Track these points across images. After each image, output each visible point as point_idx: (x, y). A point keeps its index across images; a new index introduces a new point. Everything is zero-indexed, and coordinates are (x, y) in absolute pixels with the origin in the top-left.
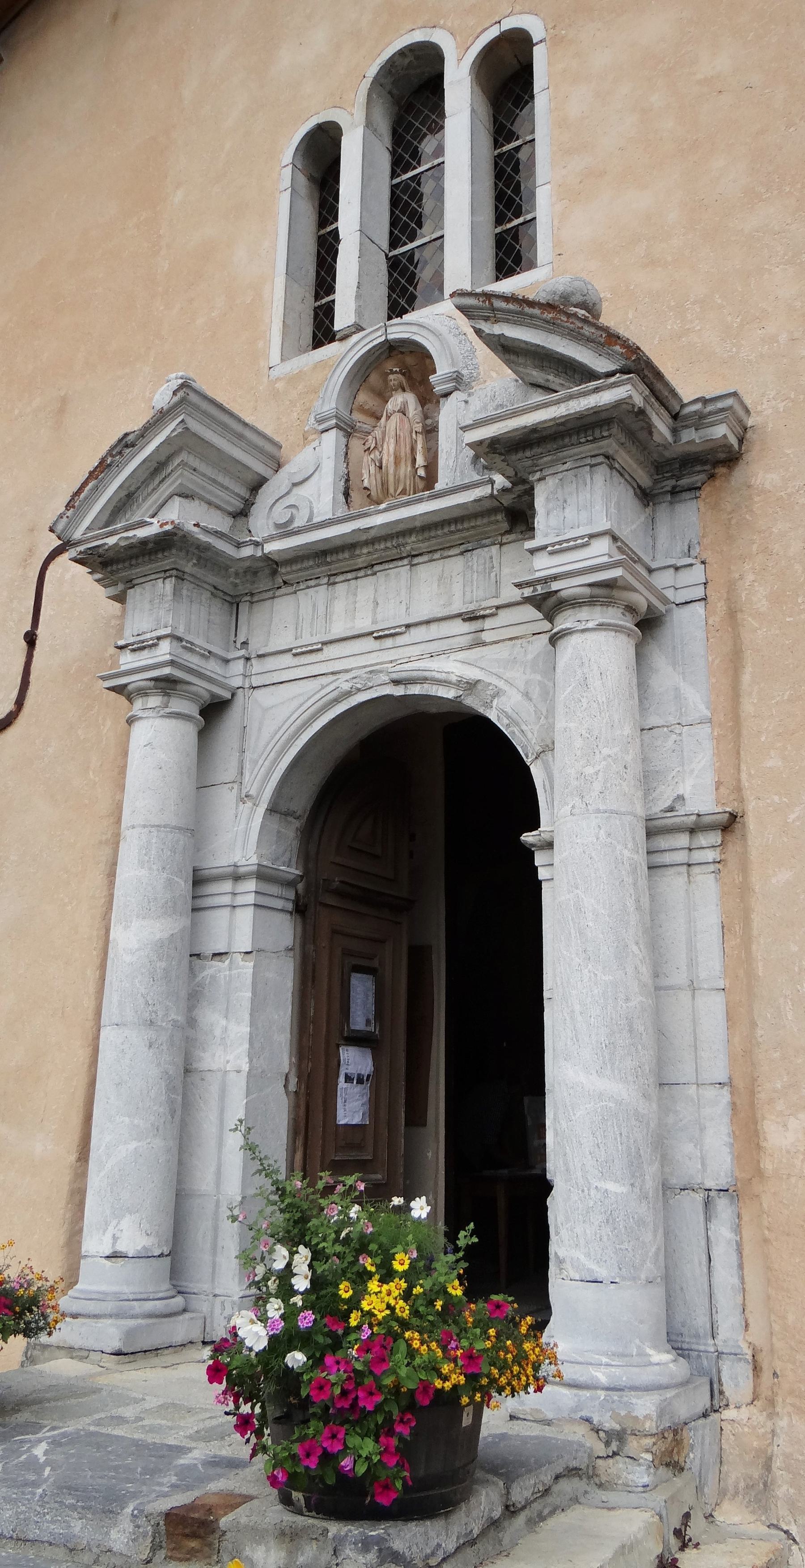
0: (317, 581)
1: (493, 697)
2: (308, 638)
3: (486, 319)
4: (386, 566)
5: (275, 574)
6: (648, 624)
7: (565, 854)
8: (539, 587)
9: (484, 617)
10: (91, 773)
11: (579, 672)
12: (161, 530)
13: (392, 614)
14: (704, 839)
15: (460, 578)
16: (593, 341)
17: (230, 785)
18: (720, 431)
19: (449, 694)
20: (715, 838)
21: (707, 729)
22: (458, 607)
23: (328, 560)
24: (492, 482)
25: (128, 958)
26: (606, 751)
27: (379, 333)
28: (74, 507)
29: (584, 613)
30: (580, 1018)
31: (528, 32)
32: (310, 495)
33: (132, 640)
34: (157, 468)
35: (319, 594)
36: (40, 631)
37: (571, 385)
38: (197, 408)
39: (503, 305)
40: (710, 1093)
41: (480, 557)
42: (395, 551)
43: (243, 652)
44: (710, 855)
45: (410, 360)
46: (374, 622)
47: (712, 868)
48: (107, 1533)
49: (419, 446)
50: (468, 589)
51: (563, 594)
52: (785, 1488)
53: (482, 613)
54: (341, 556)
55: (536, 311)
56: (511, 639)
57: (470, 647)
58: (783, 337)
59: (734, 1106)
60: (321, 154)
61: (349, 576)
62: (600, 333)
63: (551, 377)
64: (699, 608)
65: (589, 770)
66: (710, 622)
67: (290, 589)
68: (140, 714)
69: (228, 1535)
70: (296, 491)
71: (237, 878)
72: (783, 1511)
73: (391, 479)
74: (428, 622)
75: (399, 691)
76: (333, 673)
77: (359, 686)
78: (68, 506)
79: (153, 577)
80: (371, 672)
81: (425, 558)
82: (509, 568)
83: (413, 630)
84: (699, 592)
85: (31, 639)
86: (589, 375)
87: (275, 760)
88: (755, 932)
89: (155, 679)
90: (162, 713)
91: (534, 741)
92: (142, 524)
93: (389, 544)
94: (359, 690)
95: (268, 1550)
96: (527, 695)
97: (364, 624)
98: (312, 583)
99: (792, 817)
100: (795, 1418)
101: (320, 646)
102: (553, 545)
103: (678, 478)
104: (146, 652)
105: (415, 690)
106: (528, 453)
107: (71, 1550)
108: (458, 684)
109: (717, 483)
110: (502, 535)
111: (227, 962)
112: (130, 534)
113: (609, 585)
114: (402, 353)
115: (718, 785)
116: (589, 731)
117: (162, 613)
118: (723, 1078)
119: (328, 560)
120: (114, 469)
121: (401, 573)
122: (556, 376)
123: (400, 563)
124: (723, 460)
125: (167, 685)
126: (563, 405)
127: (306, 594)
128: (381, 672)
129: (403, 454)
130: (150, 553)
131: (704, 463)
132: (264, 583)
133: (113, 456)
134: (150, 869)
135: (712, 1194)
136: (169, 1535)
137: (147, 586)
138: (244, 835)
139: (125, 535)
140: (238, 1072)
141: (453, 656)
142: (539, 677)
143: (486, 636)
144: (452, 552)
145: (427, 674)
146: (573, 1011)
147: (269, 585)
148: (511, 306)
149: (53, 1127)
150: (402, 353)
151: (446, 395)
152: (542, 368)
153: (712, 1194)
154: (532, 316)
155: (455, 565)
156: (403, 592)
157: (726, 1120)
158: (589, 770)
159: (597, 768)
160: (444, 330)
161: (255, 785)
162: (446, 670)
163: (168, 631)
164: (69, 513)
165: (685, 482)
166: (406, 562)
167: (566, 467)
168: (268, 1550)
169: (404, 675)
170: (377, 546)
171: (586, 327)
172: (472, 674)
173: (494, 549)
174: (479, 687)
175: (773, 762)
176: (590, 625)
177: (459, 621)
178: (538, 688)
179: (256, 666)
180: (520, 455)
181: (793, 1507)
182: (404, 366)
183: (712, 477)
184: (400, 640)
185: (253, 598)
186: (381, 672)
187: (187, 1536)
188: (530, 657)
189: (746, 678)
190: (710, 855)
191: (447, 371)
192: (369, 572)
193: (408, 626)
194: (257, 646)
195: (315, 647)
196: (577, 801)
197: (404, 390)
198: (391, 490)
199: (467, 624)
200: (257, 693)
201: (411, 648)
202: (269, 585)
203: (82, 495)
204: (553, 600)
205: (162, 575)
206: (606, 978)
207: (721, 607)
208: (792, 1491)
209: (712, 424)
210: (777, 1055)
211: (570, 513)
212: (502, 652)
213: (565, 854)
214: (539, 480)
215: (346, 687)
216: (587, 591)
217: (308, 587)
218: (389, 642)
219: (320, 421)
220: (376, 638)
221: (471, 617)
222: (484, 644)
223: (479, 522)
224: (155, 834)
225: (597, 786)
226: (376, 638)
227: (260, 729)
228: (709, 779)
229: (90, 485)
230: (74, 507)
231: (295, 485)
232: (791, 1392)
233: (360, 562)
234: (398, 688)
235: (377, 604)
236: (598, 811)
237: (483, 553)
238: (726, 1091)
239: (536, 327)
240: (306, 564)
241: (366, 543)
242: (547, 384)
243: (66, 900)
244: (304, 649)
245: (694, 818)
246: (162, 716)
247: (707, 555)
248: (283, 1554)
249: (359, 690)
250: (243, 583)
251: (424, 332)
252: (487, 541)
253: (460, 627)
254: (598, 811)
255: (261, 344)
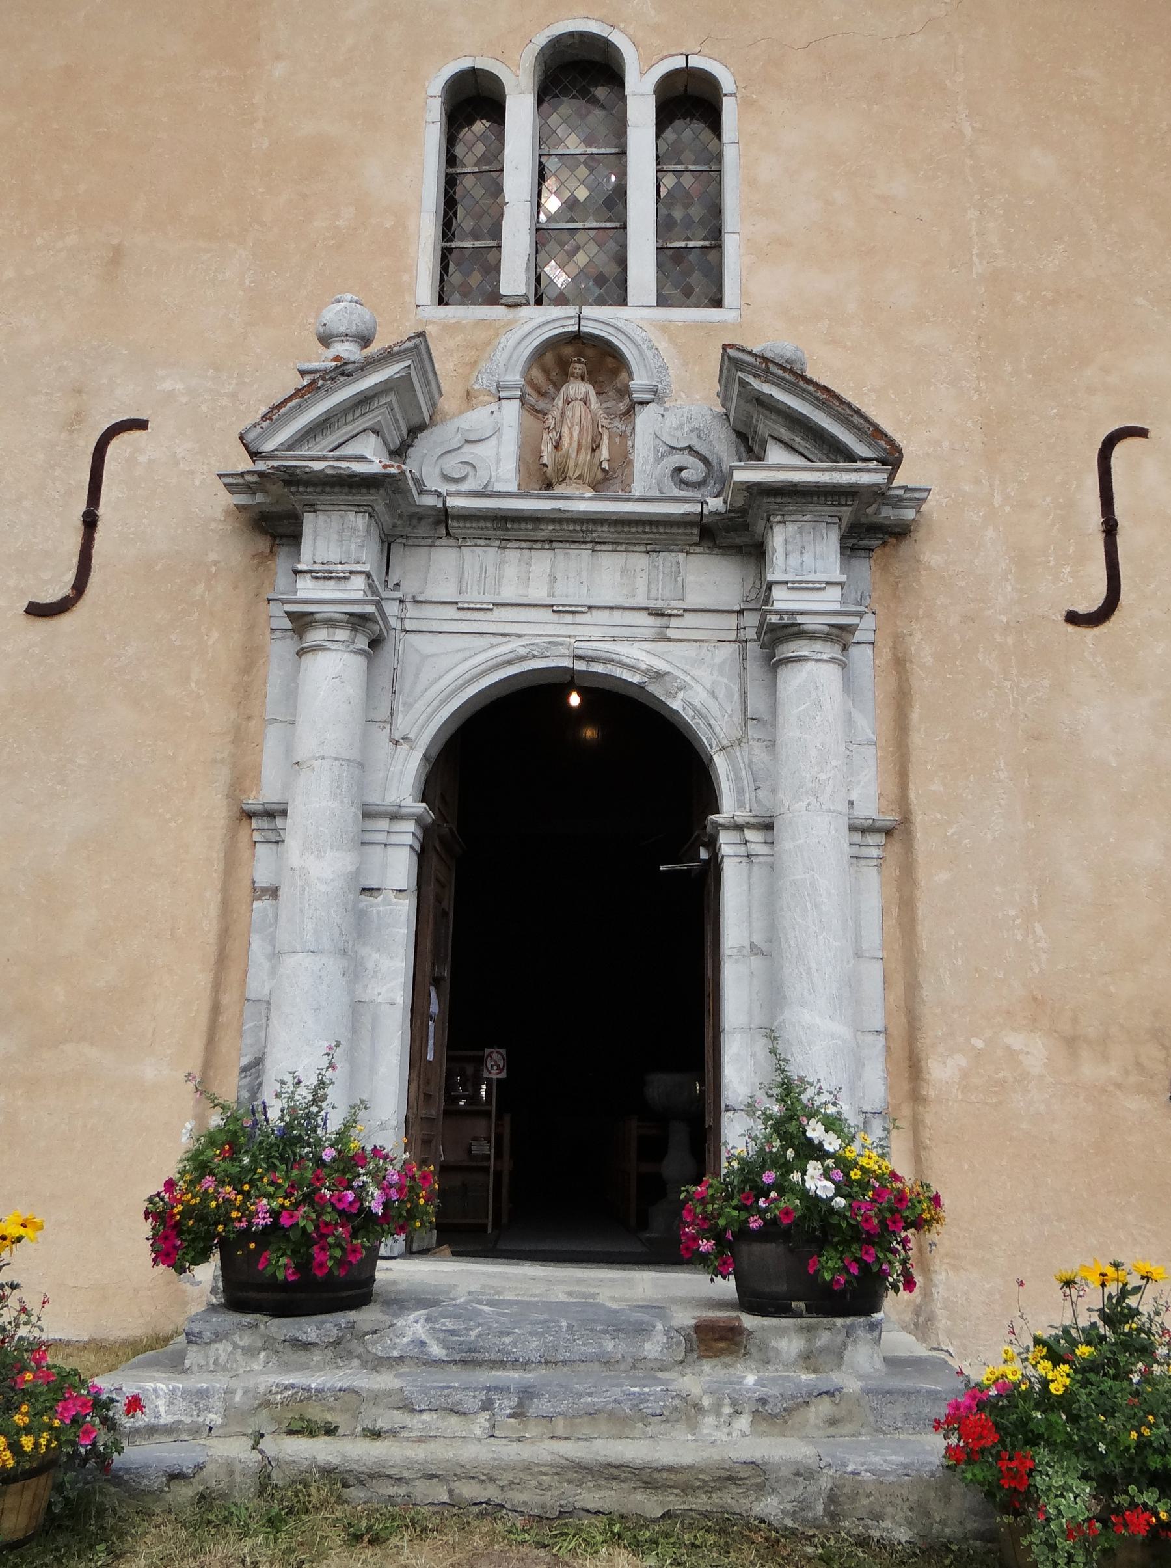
0: (487, 542)
1: (680, 689)
2: (473, 595)
3: (756, 376)
4: (567, 545)
5: (446, 524)
6: (375, 643)
7: (800, 841)
8: (785, 617)
9: (670, 615)
10: (193, 685)
11: (814, 694)
12: (384, 471)
13: (570, 593)
14: (871, 839)
15: (645, 574)
16: (859, 429)
17: (382, 725)
18: (910, 514)
19: (636, 679)
20: (880, 839)
21: (872, 749)
22: (641, 601)
23: (509, 526)
24: (703, 503)
25: (323, 888)
26: (834, 763)
27: (572, 322)
28: (271, 419)
29: (818, 646)
30: (815, 974)
31: (716, 79)
32: (483, 450)
33: (317, 567)
34: (363, 401)
35: (489, 555)
36: (103, 511)
37: (824, 458)
38: (419, 354)
39: (780, 372)
40: (870, 1038)
41: (666, 560)
42: (568, 534)
43: (398, 595)
44: (875, 852)
45: (590, 352)
46: (551, 595)
47: (875, 862)
48: (642, 1346)
49: (605, 440)
50: (653, 586)
51: (806, 627)
52: (943, 1322)
53: (669, 611)
54: (523, 526)
55: (811, 388)
56: (696, 641)
57: (654, 640)
58: (946, 445)
59: (888, 1048)
60: (473, 101)
61: (523, 545)
62: (867, 425)
63: (798, 439)
64: (868, 650)
65: (822, 776)
66: (877, 662)
67: (453, 542)
68: (328, 644)
69: (756, 1334)
70: (468, 448)
71: (395, 817)
72: (942, 1337)
73: (572, 463)
74: (611, 608)
75: (580, 666)
76: (502, 635)
77: (536, 653)
78: (264, 418)
79: (343, 508)
80: (550, 643)
81: (609, 547)
82: (710, 581)
83: (594, 612)
84: (869, 637)
85: (90, 522)
86: (851, 457)
87: (438, 707)
88: (920, 916)
89: (350, 614)
90: (351, 647)
91: (722, 735)
92: (361, 459)
93: (578, 528)
94: (534, 657)
95: (790, 1341)
96: (713, 694)
97: (538, 593)
98: (482, 542)
99: (950, 832)
100: (950, 1273)
101: (491, 606)
102: (793, 582)
103: (861, 539)
104: (332, 582)
105: (599, 668)
106: (779, 500)
107: (605, 1363)
108: (645, 673)
109: (887, 549)
110: (690, 545)
111: (380, 898)
112: (344, 465)
113: (841, 627)
114: (583, 343)
115: (880, 795)
116: (822, 744)
117: (353, 546)
118: (880, 1027)
119: (509, 526)
120: (322, 393)
121: (582, 555)
122: (803, 439)
123: (583, 546)
124: (900, 532)
125: (357, 621)
126: (827, 473)
127: (473, 552)
128: (561, 644)
129: (584, 442)
130: (350, 486)
131: (885, 533)
132: (423, 530)
133: (324, 379)
134: (342, 802)
135: (868, 1115)
136: (700, 1340)
137: (335, 516)
138: (401, 779)
139: (335, 464)
140: (392, 1004)
141: (637, 644)
142: (726, 681)
143: (670, 633)
144: (636, 548)
145: (615, 657)
146: (810, 968)
147: (431, 534)
148: (786, 376)
149: (169, 1052)
150: (583, 343)
151: (643, 403)
152: (791, 429)
153: (868, 1115)
154: (804, 390)
155: (639, 561)
156: (584, 574)
157: (882, 1059)
158: (822, 776)
159: (829, 775)
160: (638, 339)
161: (415, 729)
162: (631, 655)
163: (366, 568)
164: (264, 425)
165: (864, 543)
166: (589, 546)
167: (805, 518)
168: (790, 1341)
169: (590, 653)
170: (564, 526)
171: (855, 417)
172: (662, 666)
173: (681, 556)
174: (667, 678)
175: (936, 787)
176: (825, 657)
177: (645, 613)
178: (724, 690)
179: (411, 611)
180: (772, 499)
181: (950, 1334)
182: (586, 358)
183: (884, 543)
184: (580, 618)
185: (409, 541)
186: (561, 644)
187: (716, 1340)
188: (717, 660)
189: (915, 715)
190: (875, 852)
191: (646, 382)
192: (547, 546)
193: (590, 607)
194: (410, 588)
195: (485, 606)
196: (812, 799)
197: (583, 380)
198: (570, 473)
199: (652, 618)
200: (408, 636)
201: (592, 628)
202: (431, 534)
203: (283, 410)
204: (795, 629)
205: (356, 509)
206: (837, 944)
207: (886, 653)
208: (949, 1323)
209: (906, 507)
210: (938, 1011)
211: (808, 558)
212: (690, 650)
213: (800, 841)
214: (778, 522)
215: (523, 652)
216: (826, 629)
217: (476, 545)
218: (568, 618)
219: (499, 388)
220: (554, 611)
221: (658, 613)
222: (669, 639)
223: (674, 530)
224: (346, 767)
225: (829, 790)
226: (554, 611)
227: (417, 675)
228: (873, 791)
229: (294, 402)
230: (271, 419)
231: (467, 441)
232: (947, 1255)
233: (541, 535)
234: (579, 663)
235: (555, 578)
236: (829, 810)
237: (670, 556)
238: (882, 1038)
239: (804, 399)
240: (482, 524)
241: (553, 521)
242: (791, 443)
243: (168, 816)
244: (472, 606)
245: (871, 821)
246: (351, 651)
247: (876, 607)
248: (803, 1342)
249: (534, 657)
250: (408, 520)
251: (622, 337)
252: (675, 548)
253: (643, 619)
254: (829, 810)
255: (405, 278)
